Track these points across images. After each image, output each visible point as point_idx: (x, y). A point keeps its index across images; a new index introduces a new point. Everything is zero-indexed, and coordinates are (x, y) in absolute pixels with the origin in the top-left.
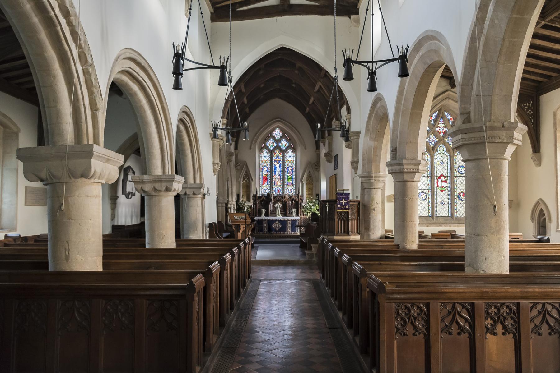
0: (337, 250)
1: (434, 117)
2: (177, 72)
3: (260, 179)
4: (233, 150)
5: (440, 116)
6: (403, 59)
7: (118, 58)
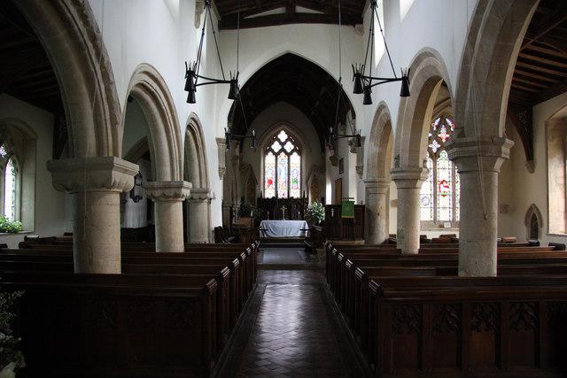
0: (341, 256)
1: (436, 123)
2: (190, 88)
3: (264, 182)
4: (238, 154)
5: (443, 122)
6: (405, 80)
7: (135, 73)
